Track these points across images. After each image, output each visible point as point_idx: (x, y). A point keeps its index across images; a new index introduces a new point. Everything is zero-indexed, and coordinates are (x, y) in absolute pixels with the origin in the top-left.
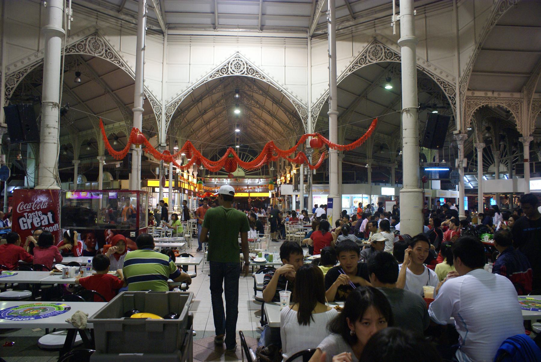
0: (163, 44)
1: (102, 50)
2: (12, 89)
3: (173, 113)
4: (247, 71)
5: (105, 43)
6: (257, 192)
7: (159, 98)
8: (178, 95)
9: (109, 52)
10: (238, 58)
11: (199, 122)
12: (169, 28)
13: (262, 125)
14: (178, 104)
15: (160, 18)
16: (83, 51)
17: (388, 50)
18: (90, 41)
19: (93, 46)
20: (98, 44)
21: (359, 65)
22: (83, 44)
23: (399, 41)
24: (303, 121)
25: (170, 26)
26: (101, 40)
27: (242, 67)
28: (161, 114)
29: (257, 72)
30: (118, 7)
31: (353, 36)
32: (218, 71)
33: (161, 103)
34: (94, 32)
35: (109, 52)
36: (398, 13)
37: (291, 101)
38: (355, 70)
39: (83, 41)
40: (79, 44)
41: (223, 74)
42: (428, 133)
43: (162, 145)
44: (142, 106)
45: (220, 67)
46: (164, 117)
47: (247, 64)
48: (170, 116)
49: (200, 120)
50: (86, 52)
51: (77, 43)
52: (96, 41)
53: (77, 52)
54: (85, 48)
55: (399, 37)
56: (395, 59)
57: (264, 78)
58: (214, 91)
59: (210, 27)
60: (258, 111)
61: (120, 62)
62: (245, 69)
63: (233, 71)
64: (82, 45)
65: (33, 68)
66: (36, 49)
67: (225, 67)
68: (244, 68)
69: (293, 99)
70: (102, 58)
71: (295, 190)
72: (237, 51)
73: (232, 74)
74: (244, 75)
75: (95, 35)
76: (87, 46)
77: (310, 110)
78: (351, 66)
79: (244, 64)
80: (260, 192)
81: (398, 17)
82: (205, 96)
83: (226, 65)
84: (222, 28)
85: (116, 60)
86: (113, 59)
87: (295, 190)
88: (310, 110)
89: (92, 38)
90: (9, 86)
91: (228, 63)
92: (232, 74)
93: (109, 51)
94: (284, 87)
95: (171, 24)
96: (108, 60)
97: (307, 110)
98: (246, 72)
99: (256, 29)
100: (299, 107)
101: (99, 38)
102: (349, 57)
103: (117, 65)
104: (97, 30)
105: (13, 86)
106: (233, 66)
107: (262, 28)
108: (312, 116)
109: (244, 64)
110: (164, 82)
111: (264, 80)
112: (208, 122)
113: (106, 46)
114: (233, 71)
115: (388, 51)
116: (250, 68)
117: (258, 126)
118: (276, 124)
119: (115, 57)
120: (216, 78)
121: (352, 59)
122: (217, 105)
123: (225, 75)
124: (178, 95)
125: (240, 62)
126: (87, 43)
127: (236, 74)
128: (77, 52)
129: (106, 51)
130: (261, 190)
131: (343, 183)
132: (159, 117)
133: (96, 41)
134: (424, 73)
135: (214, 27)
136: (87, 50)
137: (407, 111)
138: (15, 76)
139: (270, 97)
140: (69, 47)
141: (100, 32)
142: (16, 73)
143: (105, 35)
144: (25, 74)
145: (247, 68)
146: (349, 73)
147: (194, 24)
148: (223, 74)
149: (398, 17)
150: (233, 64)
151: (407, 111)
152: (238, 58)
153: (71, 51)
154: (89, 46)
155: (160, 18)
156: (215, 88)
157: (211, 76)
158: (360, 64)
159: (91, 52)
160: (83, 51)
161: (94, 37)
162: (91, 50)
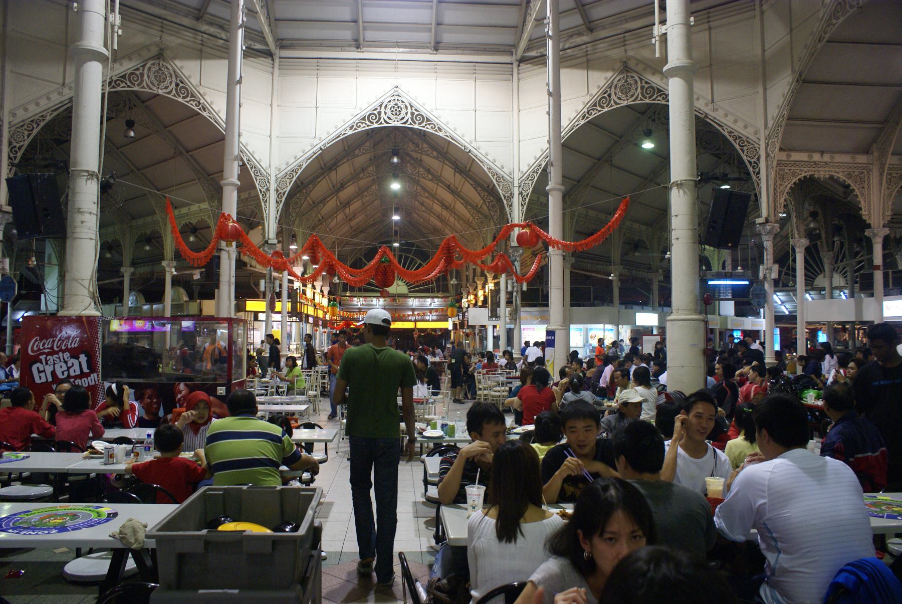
0: (273, 73)
1: (171, 83)
2: (20, 148)
3: (289, 188)
4: (412, 119)
5: (174, 71)
6: (428, 321)
7: (265, 164)
8: (296, 159)
9: (182, 87)
10: (396, 98)
11: (331, 204)
12: (282, 47)
13: (437, 208)
14: (296, 173)
15: (266, 30)
16: (138, 85)
17: (646, 83)
18: (149, 69)
19: (155, 77)
20: (163, 73)
21: (599, 108)
22: (138, 73)
23: (665, 69)
24: (505, 202)
25: (283, 44)
26: (169, 67)
27: (404, 111)
28: (268, 190)
29: (428, 120)
30: (197, 12)
31: (588, 61)
32: (364, 119)
33: (268, 171)
34: (157, 53)
35: (181, 86)
36: (663, 22)
37: (486, 169)
38: (592, 117)
39: (138, 69)
40: (132, 74)
41: (372, 123)
42: (714, 222)
43: (270, 242)
44: (236, 176)
45: (366, 112)
46: (273, 196)
47: (411, 107)
48: (284, 194)
49: (333, 201)
50: (143, 87)
51: (129, 72)
52: (160, 69)
53: (129, 86)
54: (142, 81)
55: (666, 61)
56: (659, 98)
57: (440, 130)
58: (357, 152)
59: (350, 46)
60: (430, 185)
61: (199, 103)
62: (409, 114)
63: (389, 118)
64: (136, 75)
65: (55, 113)
66: (61, 81)
67: (376, 112)
68: (406, 114)
69: (488, 165)
70: (170, 96)
71: (491, 317)
72: (396, 84)
73: (387, 123)
74: (406, 125)
75: (159, 58)
76: (146, 77)
77: (516, 184)
78: (586, 110)
79: (406, 107)
80: (433, 321)
81: (663, 29)
82: (342, 159)
83: (376, 109)
84: (370, 46)
85: (194, 101)
86: (188, 99)
87: (491, 317)
88: (516, 184)
89: (154, 64)
90: (15, 144)
91: (381, 106)
92: (387, 123)
93: (181, 85)
94: (474, 144)
95: (285, 39)
96: (180, 100)
97: (513, 183)
98: (410, 121)
99: (427, 48)
100: (499, 178)
101: (165, 64)
102: (581, 95)
103: (196, 108)
104: (162, 49)
105: (22, 143)
106: (388, 111)
107: (437, 46)
108: (521, 193)
109: (406, 107)
110: (273, 136)
111: (441, 134)
112: (347, 204)
113: (176, 77)
114: (389, 118)
115: (647, 86)
116: (416, 113)
117: (430, 211)
118: (460, 207)
119: (192, 96)
120: (360, 129)
121: (587, 99)
122: (362, 175)
123: (375, 126)
124: (296, 159)
125: (400, 104)
126: (146, 71)
127: (393, 124)
128: (129, 86)
129: (177, 85)
130: (435, 317)
131: (572, 305)
132: (264, 195)
133: (160, 69)
134: (707, 122)
135: (357, 44)
136: (144, 84)
137: (679, 185)
138: (25, 127)
139: (450, 162)
140: (114, 78)
141: (167, 53)
142: (27, 122)
143: (175, 58)
144: (42, 124)
145: (412, 114)
146: (582, 122)
147: (323, 40)
148: (372, 123)
149: (663, 29)
150: (389, 106)
151: (679, 185)
152: (396, 98)
153: (119, 85)
154: (149, 77)
155: (266, 30)
156: (359, 147)
157: (351, 128)
158: (600, 106)
159: (151, 86)
160: (138, 85)
161: (157, 61)
162: (152, 83)
